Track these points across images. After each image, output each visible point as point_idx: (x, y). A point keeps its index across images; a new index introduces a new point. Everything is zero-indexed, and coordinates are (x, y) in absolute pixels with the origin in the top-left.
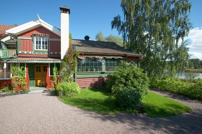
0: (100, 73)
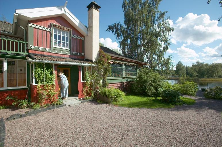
0: (122, 78)
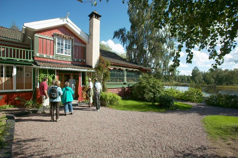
0: (123, 84)
